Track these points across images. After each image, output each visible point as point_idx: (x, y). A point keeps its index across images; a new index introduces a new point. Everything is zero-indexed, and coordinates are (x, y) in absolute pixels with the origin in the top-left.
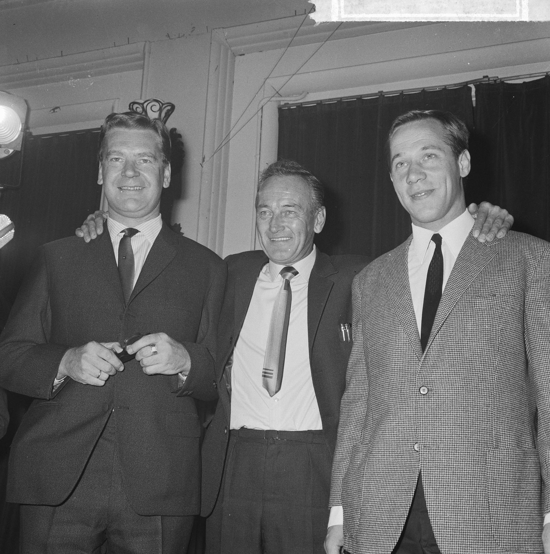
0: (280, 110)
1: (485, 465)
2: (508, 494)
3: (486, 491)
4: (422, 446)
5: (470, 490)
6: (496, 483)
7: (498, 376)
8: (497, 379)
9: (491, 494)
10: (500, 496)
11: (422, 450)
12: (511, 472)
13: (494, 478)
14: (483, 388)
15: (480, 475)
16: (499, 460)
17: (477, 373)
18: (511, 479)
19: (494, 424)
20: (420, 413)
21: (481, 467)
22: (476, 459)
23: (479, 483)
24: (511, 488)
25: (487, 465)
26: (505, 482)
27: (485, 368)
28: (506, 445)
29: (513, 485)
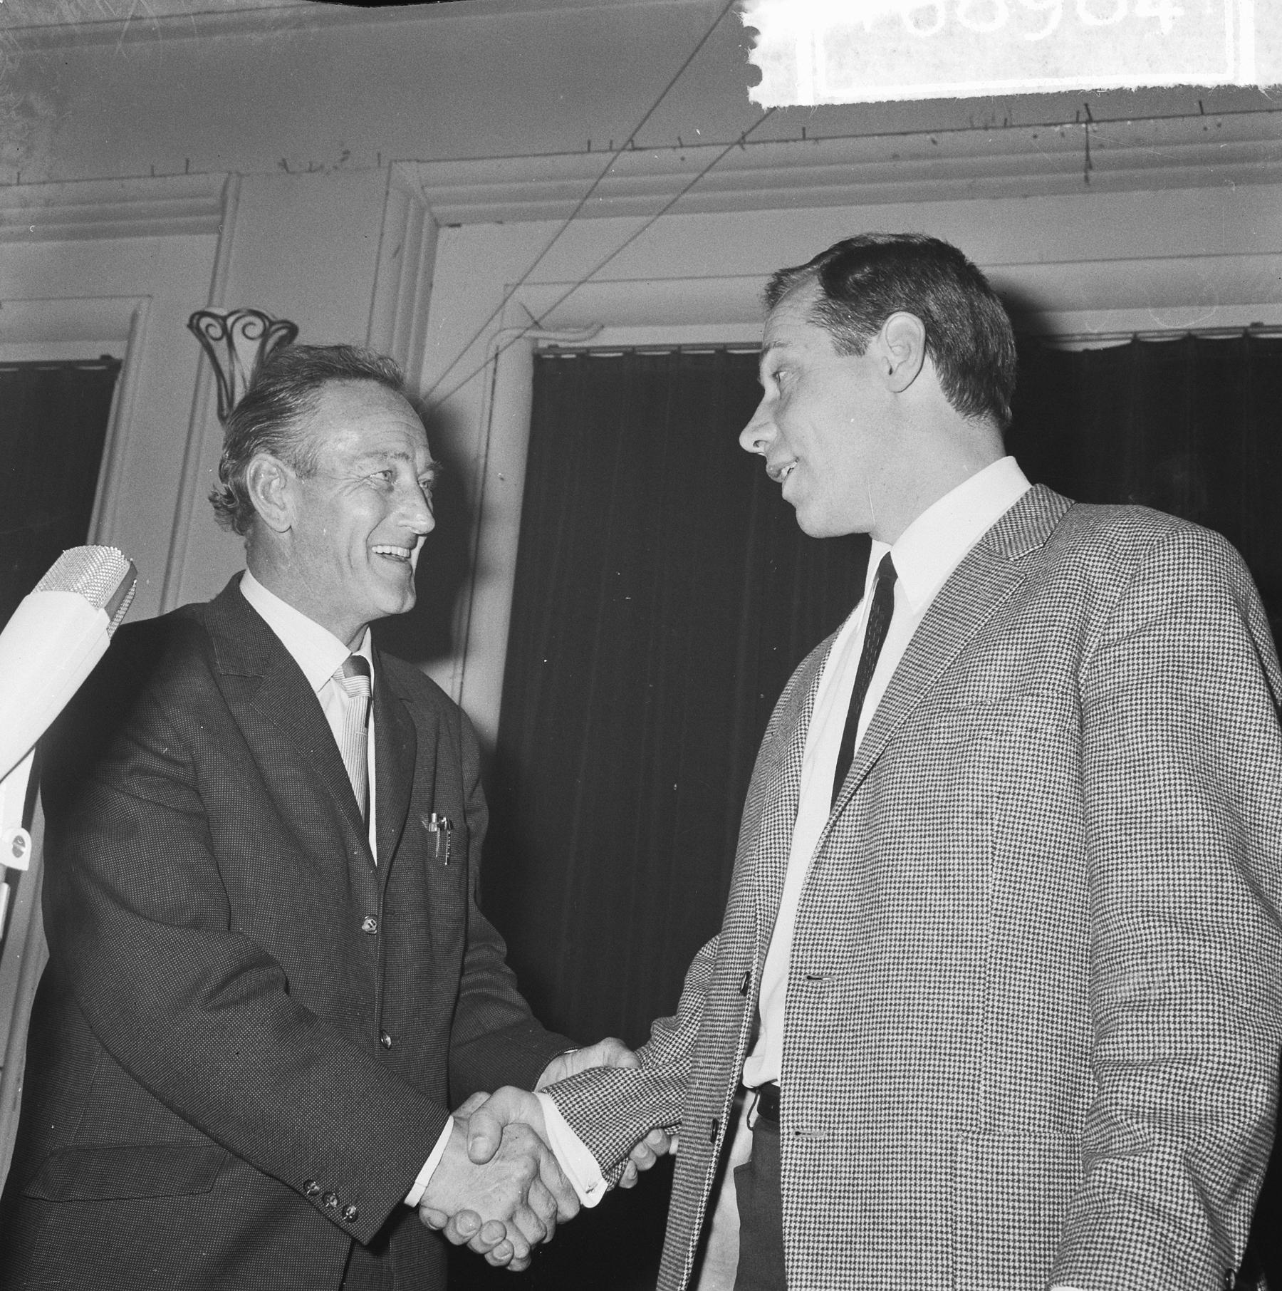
0: (539, 360)
1: (951, 1180)
2: (1014, 1267)
3: (947, 1259)
4: (791, 1130)
5: (903, 1254)
6: (980, 1234)
7: (997, 925)
8: (994, 933)
9: (964, 1267)
10: (988, 1272)
11: (790, 1143)
12: (1024, 1201)
13: (974, 1220)
14: (954, 962)
15: (931, 1212)
16: (992, 1166)
17: (937, 920)
18: (1025, 1221)
19: (984, 1063)
20: (793, 1040)
21: (936, 1186)
22: (923, 1163)
23: (929, 1235)
24: (1025, 1248)
25: (955, 1182)
26: (1006, 1230)
27: (958, 905)
28: (1019, 1122)
29: (1030, 1242)
